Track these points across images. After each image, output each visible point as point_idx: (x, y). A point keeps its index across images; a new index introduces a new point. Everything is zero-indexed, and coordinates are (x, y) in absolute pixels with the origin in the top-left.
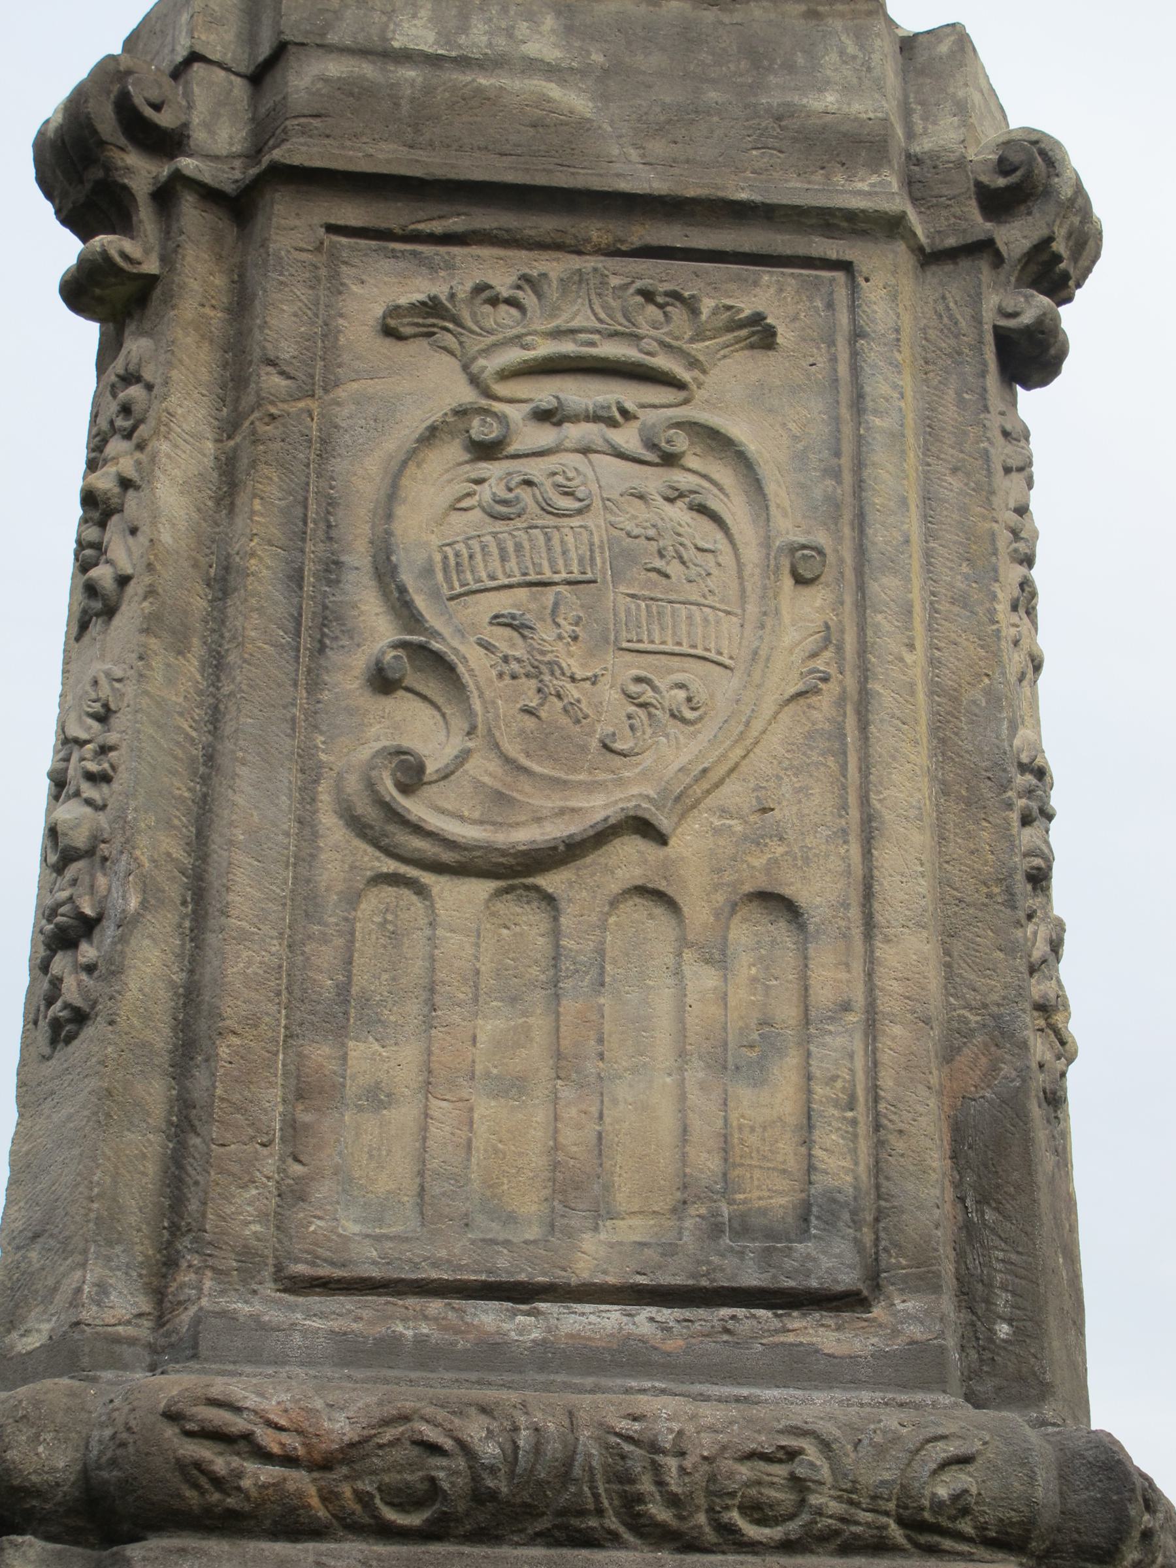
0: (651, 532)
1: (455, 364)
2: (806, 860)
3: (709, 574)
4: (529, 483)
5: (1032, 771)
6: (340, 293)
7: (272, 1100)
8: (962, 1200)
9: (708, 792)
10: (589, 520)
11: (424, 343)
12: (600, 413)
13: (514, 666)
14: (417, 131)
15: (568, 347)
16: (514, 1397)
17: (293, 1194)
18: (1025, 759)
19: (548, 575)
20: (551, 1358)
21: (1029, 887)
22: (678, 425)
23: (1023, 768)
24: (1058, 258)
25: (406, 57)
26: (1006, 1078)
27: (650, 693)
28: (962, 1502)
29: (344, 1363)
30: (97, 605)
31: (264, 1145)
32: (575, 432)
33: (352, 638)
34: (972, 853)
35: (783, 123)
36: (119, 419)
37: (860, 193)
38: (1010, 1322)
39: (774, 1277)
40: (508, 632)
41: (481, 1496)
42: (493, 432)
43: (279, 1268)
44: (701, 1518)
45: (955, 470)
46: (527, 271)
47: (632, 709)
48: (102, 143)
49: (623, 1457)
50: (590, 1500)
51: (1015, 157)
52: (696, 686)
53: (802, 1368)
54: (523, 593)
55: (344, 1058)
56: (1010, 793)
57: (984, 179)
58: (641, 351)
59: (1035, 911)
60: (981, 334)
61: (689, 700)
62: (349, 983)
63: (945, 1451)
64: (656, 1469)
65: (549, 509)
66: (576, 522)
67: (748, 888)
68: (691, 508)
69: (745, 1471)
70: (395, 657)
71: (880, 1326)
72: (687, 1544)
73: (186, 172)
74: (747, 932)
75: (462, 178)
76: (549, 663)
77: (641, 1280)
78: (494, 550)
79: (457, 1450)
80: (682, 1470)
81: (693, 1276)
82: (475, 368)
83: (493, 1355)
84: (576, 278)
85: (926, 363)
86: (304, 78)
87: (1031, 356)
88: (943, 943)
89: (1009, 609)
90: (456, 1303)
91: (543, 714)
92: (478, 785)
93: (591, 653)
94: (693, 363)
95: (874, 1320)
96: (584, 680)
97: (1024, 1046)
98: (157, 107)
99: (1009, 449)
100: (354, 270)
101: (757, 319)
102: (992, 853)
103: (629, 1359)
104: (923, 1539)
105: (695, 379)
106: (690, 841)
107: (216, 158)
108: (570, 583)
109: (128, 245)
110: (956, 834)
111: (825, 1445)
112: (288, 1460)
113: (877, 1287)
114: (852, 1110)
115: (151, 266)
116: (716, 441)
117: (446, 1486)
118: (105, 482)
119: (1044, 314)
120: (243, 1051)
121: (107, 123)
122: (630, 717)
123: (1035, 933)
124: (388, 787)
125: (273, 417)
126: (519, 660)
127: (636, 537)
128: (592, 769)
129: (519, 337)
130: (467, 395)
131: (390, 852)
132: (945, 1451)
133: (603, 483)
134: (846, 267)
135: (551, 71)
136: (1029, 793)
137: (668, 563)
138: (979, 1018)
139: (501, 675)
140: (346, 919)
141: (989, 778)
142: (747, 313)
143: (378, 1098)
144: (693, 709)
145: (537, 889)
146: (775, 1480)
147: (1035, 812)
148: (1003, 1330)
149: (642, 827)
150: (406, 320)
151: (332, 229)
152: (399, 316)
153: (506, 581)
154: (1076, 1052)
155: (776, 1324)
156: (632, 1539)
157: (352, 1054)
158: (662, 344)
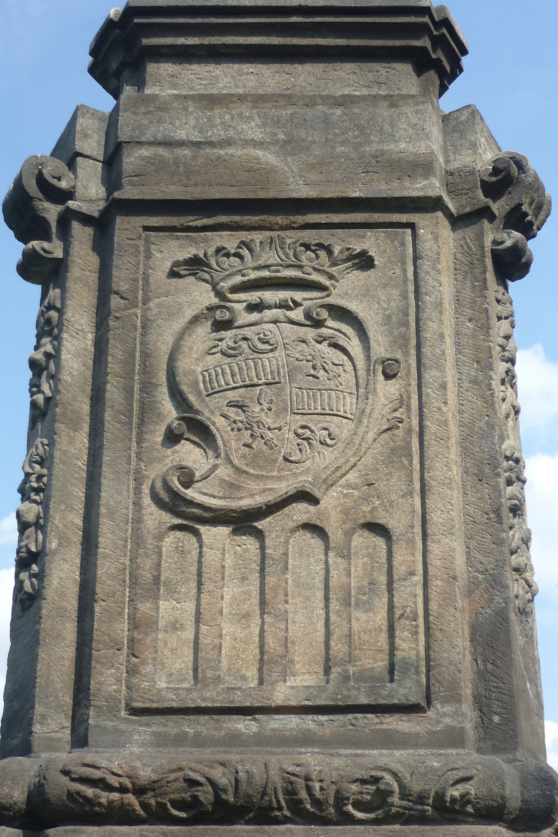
0: (309, 358)
1: (209, 287)
2: (392, 506)
3: (339, 376)
4: (245, 339)
5: (513, 460)
6: (150, 258)
7: (122, 629)
8: (476, 660)
9: (341, 478)
10: (277, 354)
11: (192, 278)
12: (282, 303)
13: (240, 424)
14: (188, 179)
15: (266, 273)
16: (237, 757)
17: (132, 671)
18: (508, 453)
19: (255, 381)
20: (261, 740)
21: (511, 514)
22: (322, 306)
23: (508, 458)
24: (527, 215)
25: (181, 144)
26: (498, 603)
27: (309, 433)
28: (466, 798)
29: (158, 745)
30: (37, 412)
31: (118, 650)
32: (268, 314)
33: (158, 417)
34: (480, 499)
35: (378, 159)
36: (49, 327)
37: (417, 188)
38: (499, 714)
39: (376, 699)
40: (235, 409)
41: (219, 802)
42: (227, 315)
43: (127, 705)
44: (332, 810)
45: (470, 320)
46: (244, 239)
47: (300, 441)
48: (31, 199)
49: (291, 783)
50: (275, 803)
51: (501, 166)
52: (333, 428)
53: (390, 740)
54: (243, 390)
55: (158, 609)
56: (499, 470)
57: (486, 178)
58: (303, 273)
59: (514, 525)
60: (483, 252)
61: (330, 435)
62: (160, 575)
63: (457, 775)
64: (309, 789)
65: (254, 350)
66: (270, 355)
67: (362, 521)
68: (330, 345)
69: (354, 787)
70: (178, 424)
71: (430, 719)
72: (324, 821)
73: (72, 208)
74: (362, 540)
75: (210, 198)
76: (257, 422)
77: (307, 703)
78: (228, 371)
79: (207, 783)
80: (322, 789)
81: (333, 699)
82: (218, 287)
83: (234, 740)
84: (269, 241)
85: (456, 270)
86: (131, 160)
87: (511, 265)
88: (465, 542)
89: (500, 384)
90: (215, 717)
91: (254, 446)
92: (222, 481)
93: (277, 415)
94: (331, 277)
95: (427, 717)
96: (275, 429)
97: (506, 587)
98: (59, 179)
99: (500, 308)
100: (158, 247)
101: (363, 253)
102: (490, 499)
103: (306, 739)
104: (447, 815)
105: (332, 285)
106: (330, 501)
107: (91, 201)
108: (267, 384)
109: (46, 245)
110: (471, 491)
111: (395, 775)
112: (123, 790)
113: (429, 702)
114: (415, 621)
115: (59, 254)
116: (341, 313)
117: (202, 799)
118: (39, 356)
119: (517, 241)
120: (106, 608)
121: (32, 188)
122: (298, 445)
123: (514, 535)
124: (176, 484)
125: (117, 318)
126: (242, 422)
127: (301, 361)
128: (280, 470)
129: (240, 271)
130: (215, 301)
131: (178, 514)
132: (457, 775)
133: (284, 336)
134: (412, 226)
135: (260, 145)
136: (511, 469)
137: (318, 372)
138: (484, 576)
139: (232, 430)
140: (158, 546)
141: (488, 464)
142: (358, 251)
143: (175, 626)
144: (331, 439)
145: (255, 527)
146: (370, 791)
147: (514, 478)
148: (496, 719)
149: (304, 496)
150: (182, 268)
151: (146, 228)
152: (178, 267)
153: (235, 385)
154: (538, 590)
155: (376, 720)
156: (299, 820)
157: (161, 607)
158: (314, 269)
